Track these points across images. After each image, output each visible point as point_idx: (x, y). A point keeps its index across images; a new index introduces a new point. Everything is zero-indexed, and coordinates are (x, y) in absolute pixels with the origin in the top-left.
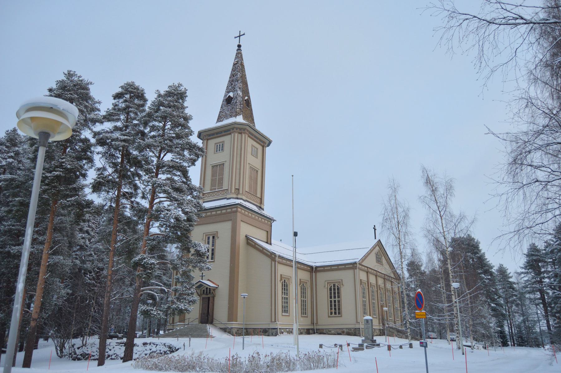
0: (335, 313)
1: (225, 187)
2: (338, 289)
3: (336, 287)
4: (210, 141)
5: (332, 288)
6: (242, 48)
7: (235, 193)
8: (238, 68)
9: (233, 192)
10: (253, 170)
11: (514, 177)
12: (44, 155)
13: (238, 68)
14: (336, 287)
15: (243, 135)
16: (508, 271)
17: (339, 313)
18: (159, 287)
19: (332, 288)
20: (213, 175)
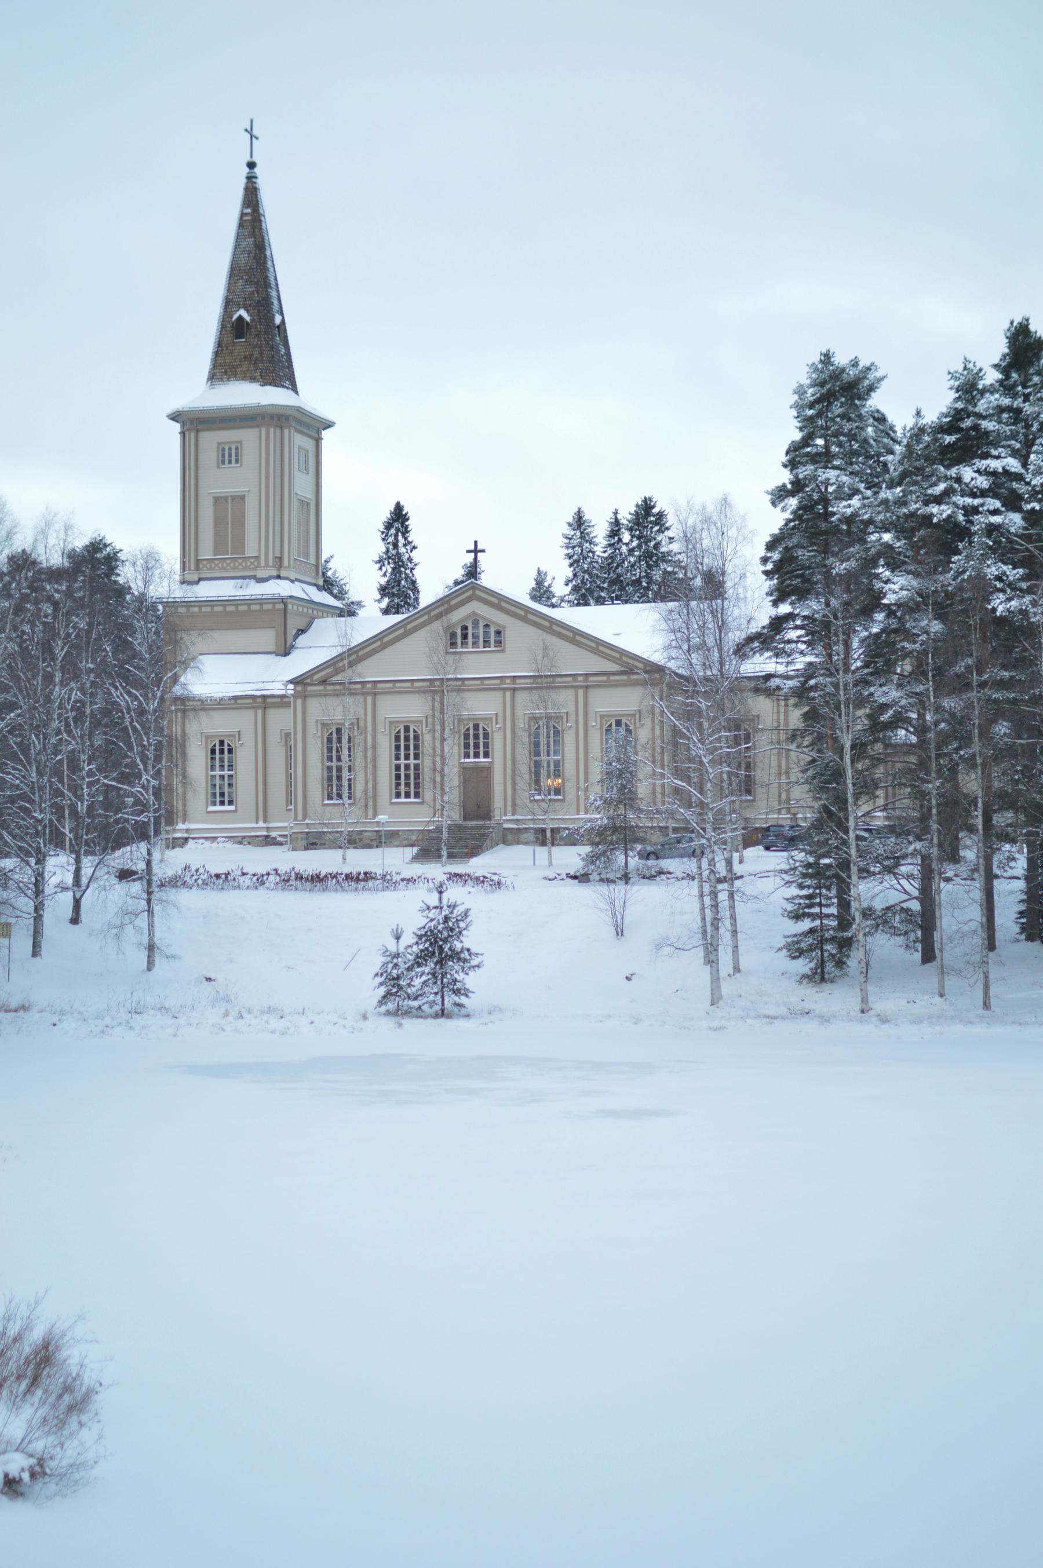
0: (486, 643)
1: (251, 550)
2: (486, 736)
3: (481, 731)
4: (203, 435)
5: (471, 732)
6: (257, 170)
7: (274, 566)
8: (251, 196)
9: (271, 564)
10: (304, 504)
11: (865, 506)
12: (333, 894)
13: (251, 196)
14: (481, 731)
15: (286, 431)
16: (64, 1354)
17: (499, 643)
18: (141, 766)
19: (471, 732)
20: (219, 521)
